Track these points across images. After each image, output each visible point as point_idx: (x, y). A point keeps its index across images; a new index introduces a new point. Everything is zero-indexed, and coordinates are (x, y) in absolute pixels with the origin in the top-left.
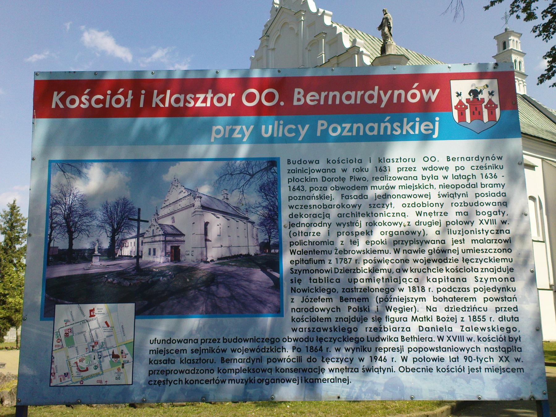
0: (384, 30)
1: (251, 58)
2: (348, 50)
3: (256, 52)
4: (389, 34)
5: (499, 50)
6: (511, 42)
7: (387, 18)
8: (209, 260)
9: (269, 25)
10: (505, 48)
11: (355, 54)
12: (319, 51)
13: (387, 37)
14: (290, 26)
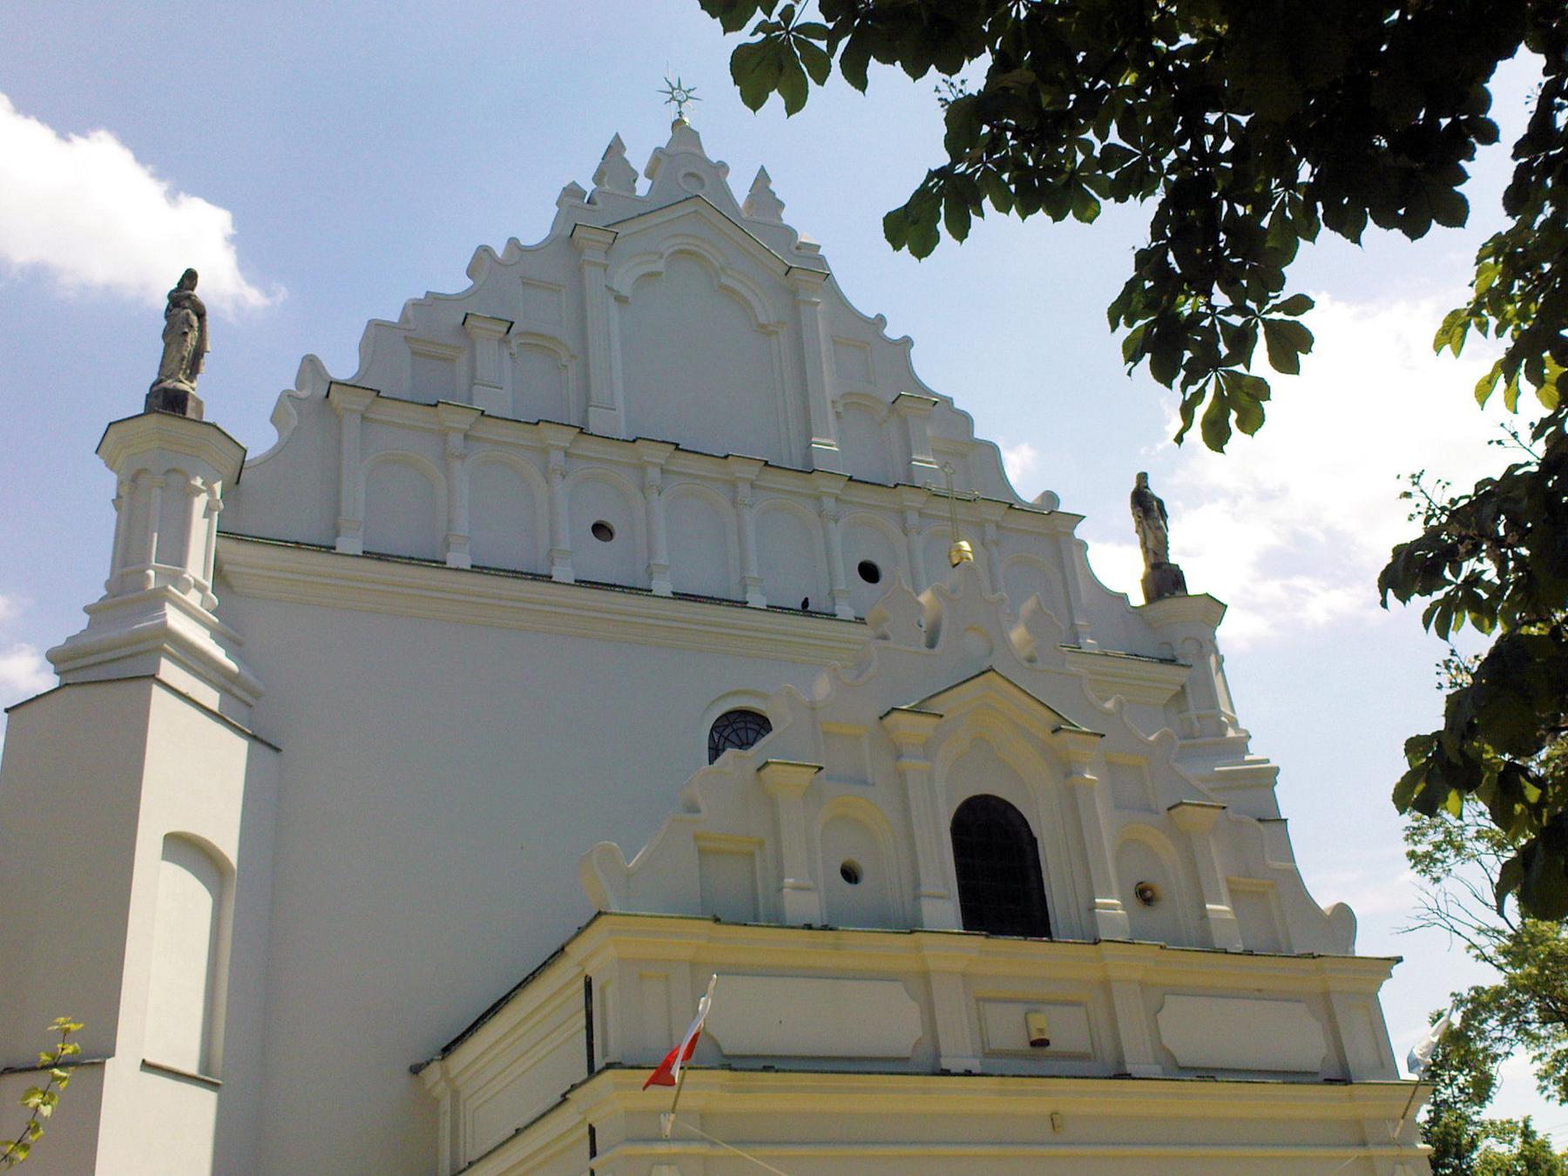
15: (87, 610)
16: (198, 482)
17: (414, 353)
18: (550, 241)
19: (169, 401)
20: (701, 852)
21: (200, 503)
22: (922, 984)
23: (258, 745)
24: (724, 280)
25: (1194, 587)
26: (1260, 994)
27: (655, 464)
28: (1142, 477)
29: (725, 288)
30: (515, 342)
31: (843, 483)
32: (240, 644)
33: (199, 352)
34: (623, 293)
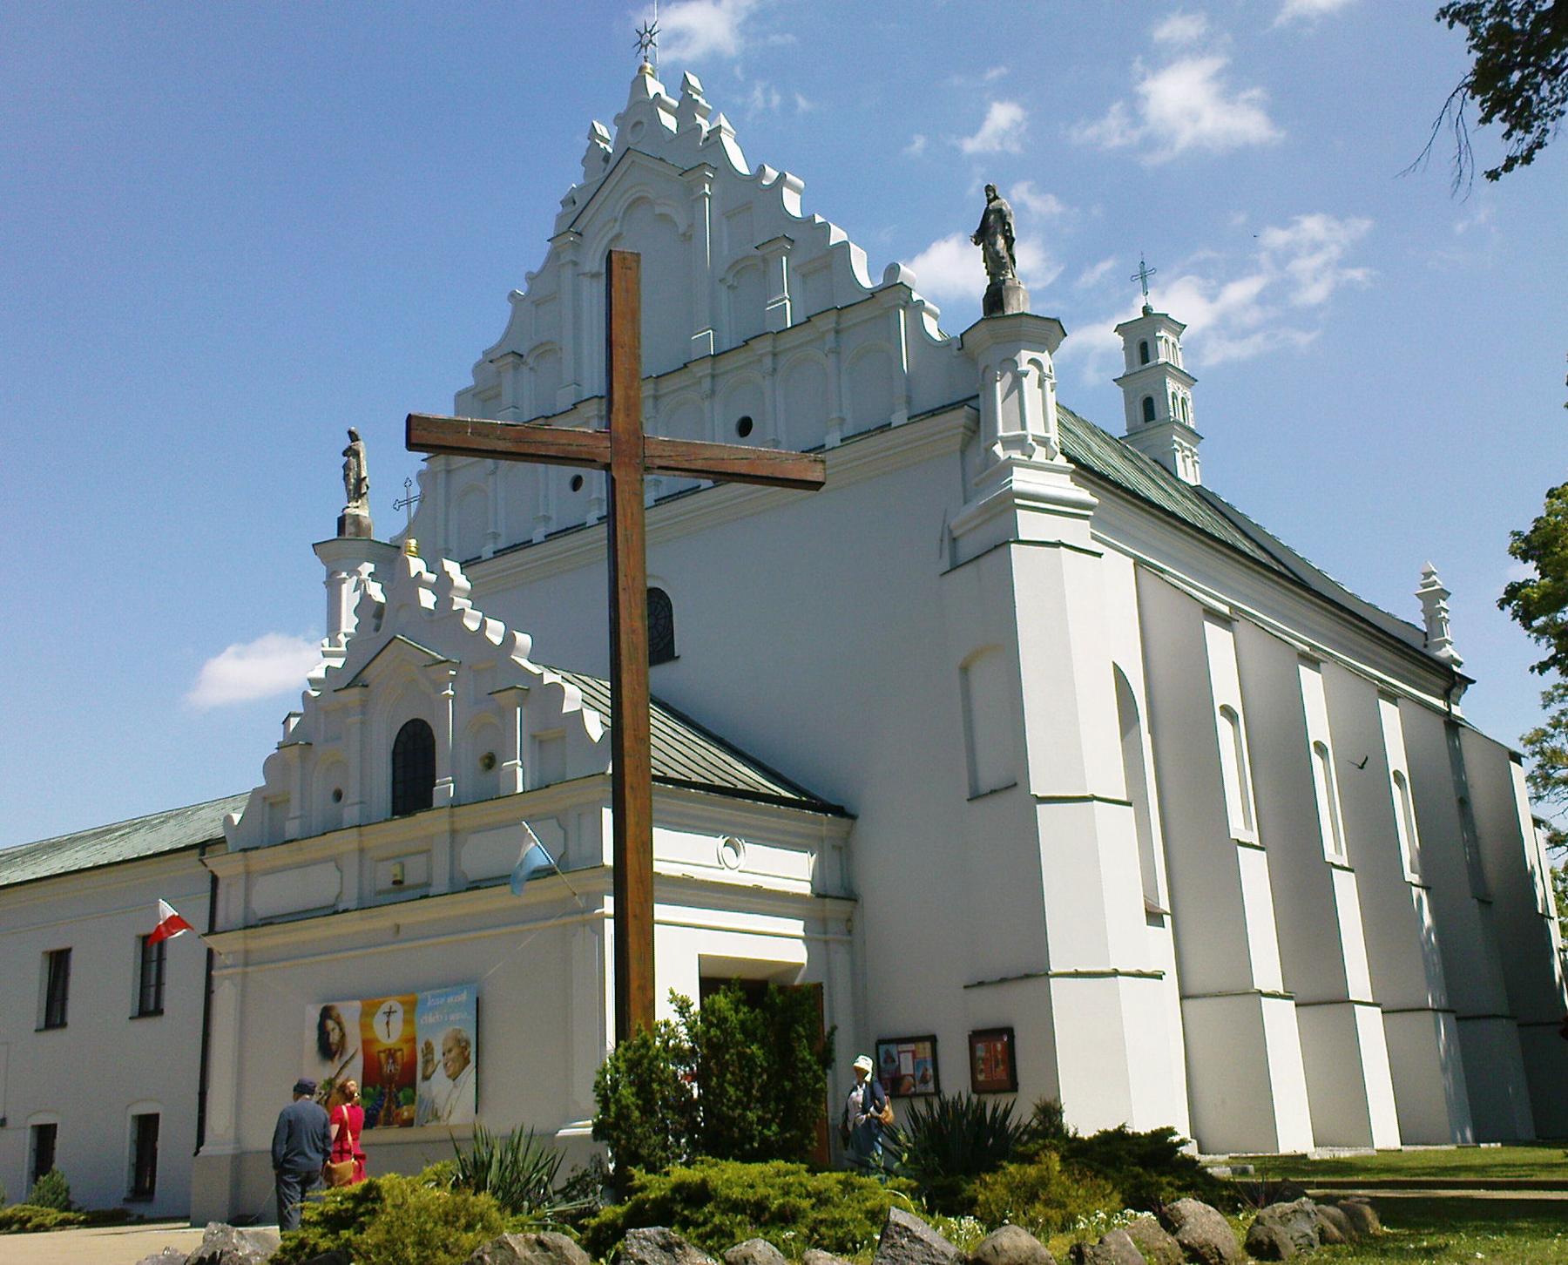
0: (994, 244)
1: (513, 295)
2: (873, 294)
3: (531, 278)
4: (1007, 259)
5: (1129, 363)
6: (1161, 344)
7: (1000, 211)
8: (292, 828)
9: (580, 204)
10: (1145, 358)
11: (895, 308)
12: (769, 287)
13: (1004, 266)
14: (658, 210)
16: (344, 575)
30: (530, 360)
33: (360, 480)
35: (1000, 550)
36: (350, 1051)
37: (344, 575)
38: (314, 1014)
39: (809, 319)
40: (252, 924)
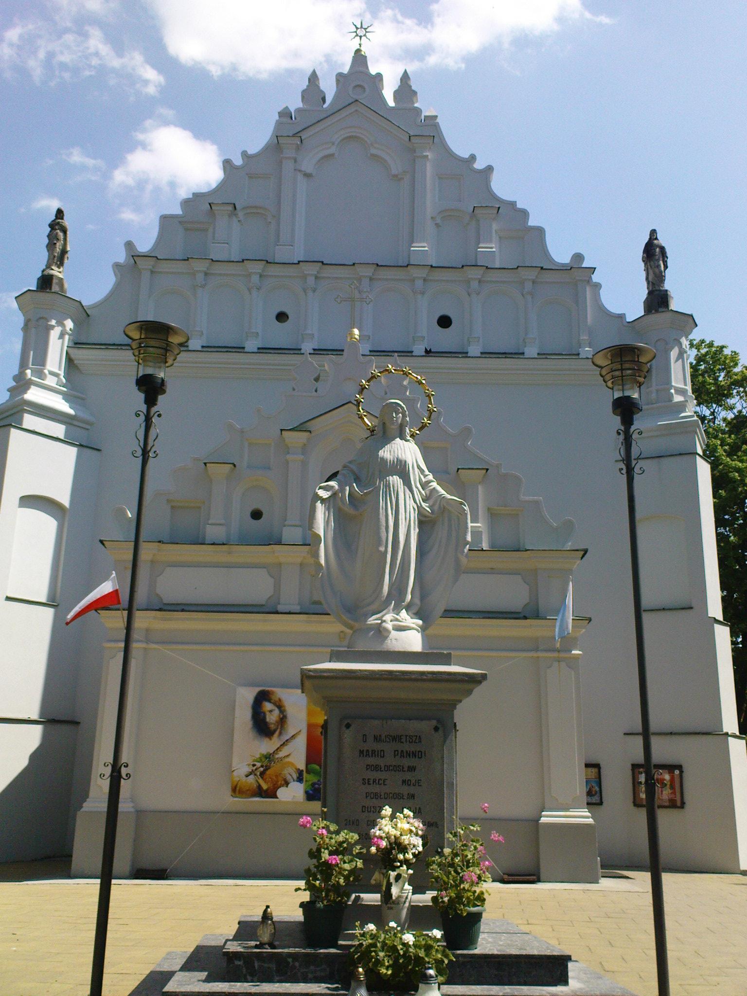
15: (8, 390)
16: (53, 322)
17: (186, 229)
18: (266, 149)
19: (46, 282)
20: (173, 507)
21: (55, 334)
22: (275, 570)
23: (82, 448)
24: (373, 151)
25: (674, 305)
26: (492, 571)
27: (312, 275)
28: (653, 232)
29: (373, 156)
30: (241, 214)
31: (427, 269)
32: (83, 399)
33: (64, 252)
34: (309, 171)
35: (691, 456)
36: (291, 731)
37: (53, 322)
38: (246, 696)
39: (243, 261)
40: (165, 607)
